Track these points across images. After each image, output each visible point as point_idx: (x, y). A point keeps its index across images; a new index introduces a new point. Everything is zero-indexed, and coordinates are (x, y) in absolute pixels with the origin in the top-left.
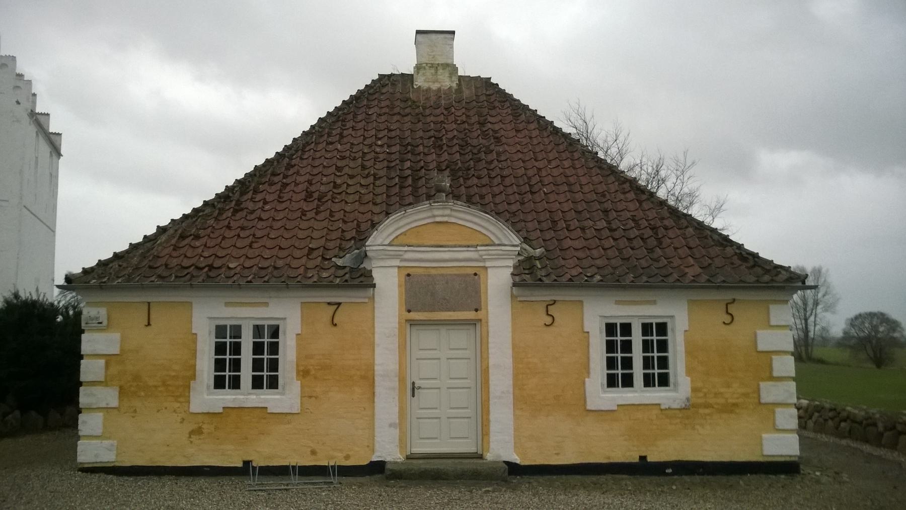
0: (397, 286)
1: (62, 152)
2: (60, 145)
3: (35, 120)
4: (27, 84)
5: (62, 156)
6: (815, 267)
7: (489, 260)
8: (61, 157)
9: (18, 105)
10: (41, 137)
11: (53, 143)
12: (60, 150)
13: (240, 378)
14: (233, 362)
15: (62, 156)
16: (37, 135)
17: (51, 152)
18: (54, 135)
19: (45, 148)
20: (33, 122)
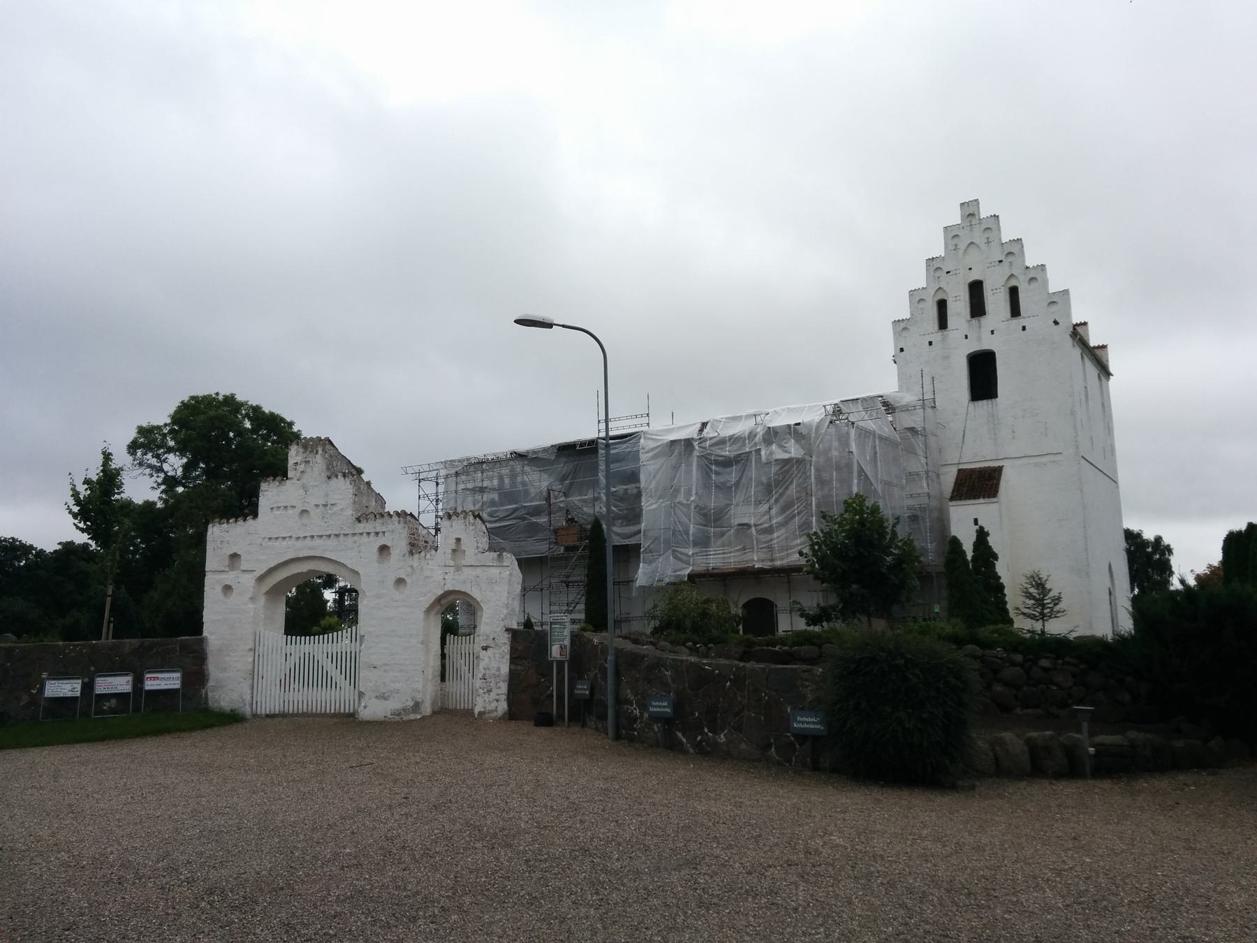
0: (331, 572)
1: (1112, 370)
2: (1107, 361)
3: (1080, 339)
4: (1064, 295)
5: (1112, 375)
6: (261, 408)
7: (1115, 622)
8: (1111, 377)
9: (1056, 327)
10: (1086, 360)
11: (1097, 358)
12: (1108, 368)
13: (999, 479)
14: (557, 699)
15: (1112, 375)
16: (1099, 378)
17: (1099, 374)
18: (1099, 350)
19: (1092, 371)
20: (1077, 343)
